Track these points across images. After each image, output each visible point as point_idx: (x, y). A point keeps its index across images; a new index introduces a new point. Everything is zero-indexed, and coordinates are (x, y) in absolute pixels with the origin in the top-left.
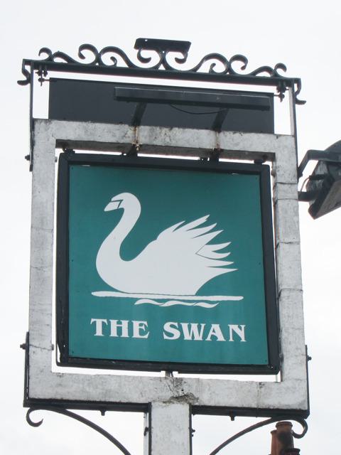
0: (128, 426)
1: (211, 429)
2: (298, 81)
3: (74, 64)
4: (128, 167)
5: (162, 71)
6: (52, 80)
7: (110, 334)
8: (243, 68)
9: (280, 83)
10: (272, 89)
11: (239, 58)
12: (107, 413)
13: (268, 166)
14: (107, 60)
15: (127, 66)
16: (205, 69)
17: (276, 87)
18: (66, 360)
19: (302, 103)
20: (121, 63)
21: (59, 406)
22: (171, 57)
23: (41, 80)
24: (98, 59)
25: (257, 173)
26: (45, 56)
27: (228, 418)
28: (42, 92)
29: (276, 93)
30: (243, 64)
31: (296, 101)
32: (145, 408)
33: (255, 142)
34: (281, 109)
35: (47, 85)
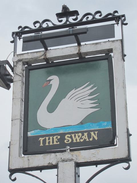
0: (49, 175)
1: (86, 172)
2: (123, 16)
3: (56, 26)
4: (51, 66)
5: (68, 25)
6: (23, 38)
7: (87, 134)
8: (100, 16)
9: (115, 18)
10: (114, 22)
11: (97, 12)
12: (43, 171)
13: (111, 55)
14: (97, 17)
15: (53, 25)
16: (85, 20)
17: (114, 21)
18: (112, 144)
19: (126, 24)
20: (50, 25)
21: (23, 170)
22: (71, 19)
23: (20, 39)
24: (94, 18)
25: (107, 59)
26: (38, 25)
27: (39, 171)
28: (20, 43)
29: (115, 23)
30: (99, 14)
31: (123, 24)
32: (55, 167)
33: (104, 44)
34: (118, 28)
35: (22, 40)
